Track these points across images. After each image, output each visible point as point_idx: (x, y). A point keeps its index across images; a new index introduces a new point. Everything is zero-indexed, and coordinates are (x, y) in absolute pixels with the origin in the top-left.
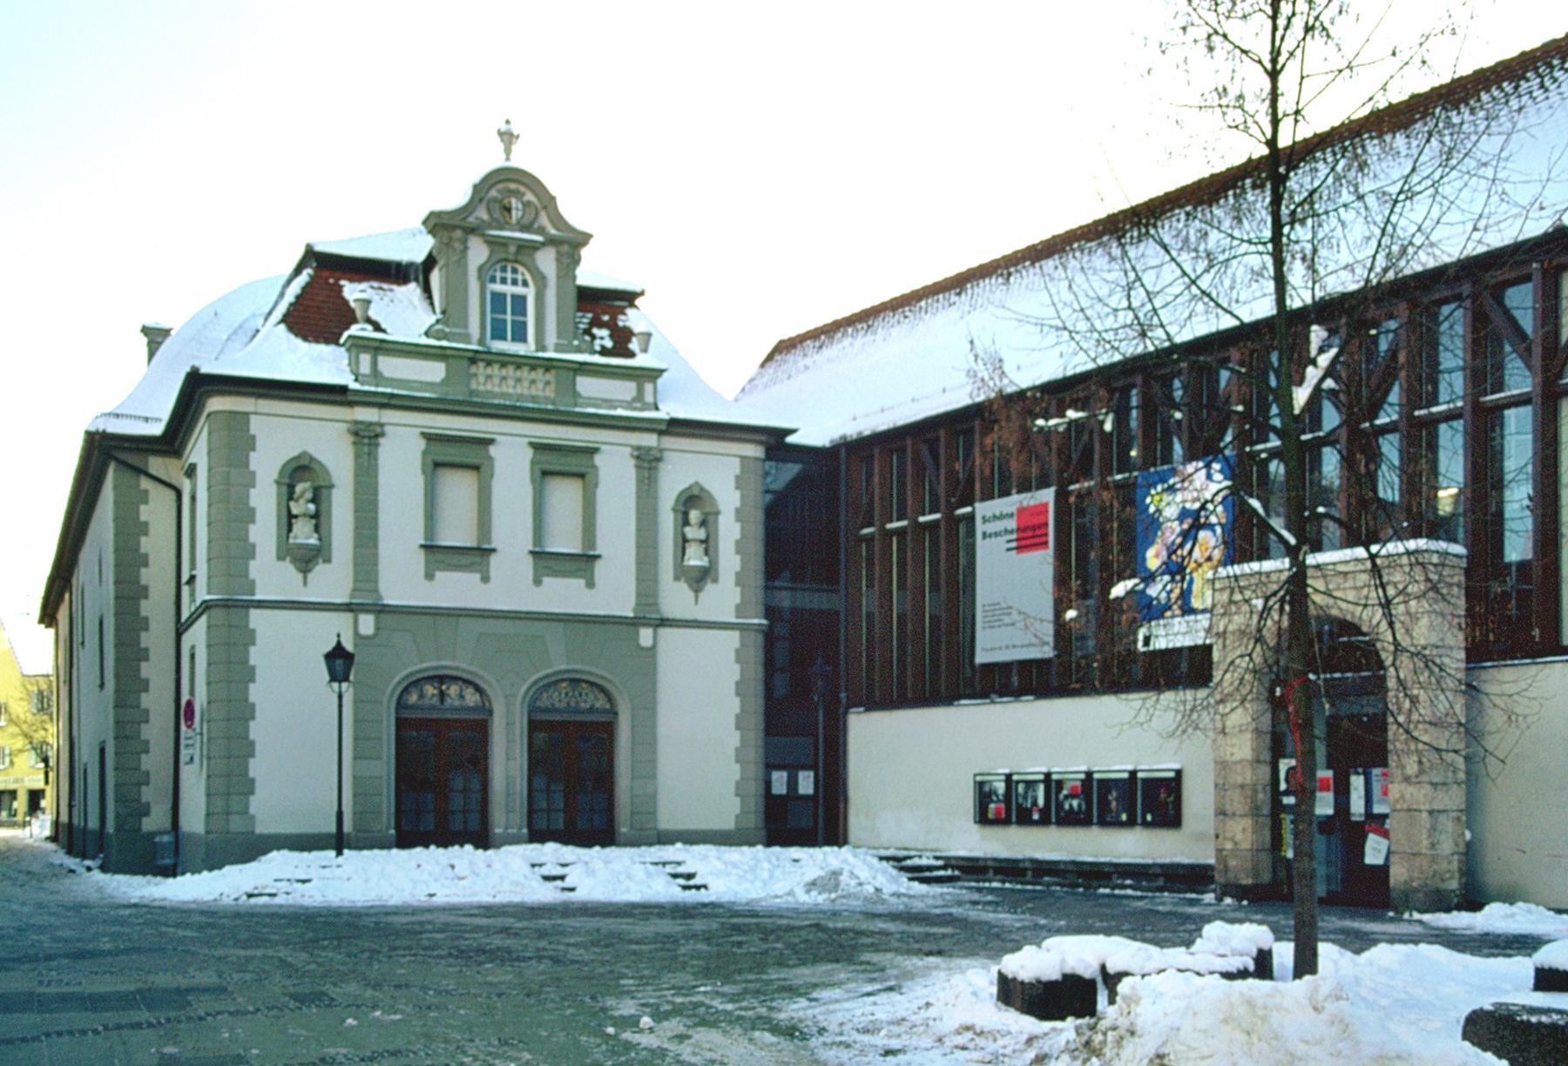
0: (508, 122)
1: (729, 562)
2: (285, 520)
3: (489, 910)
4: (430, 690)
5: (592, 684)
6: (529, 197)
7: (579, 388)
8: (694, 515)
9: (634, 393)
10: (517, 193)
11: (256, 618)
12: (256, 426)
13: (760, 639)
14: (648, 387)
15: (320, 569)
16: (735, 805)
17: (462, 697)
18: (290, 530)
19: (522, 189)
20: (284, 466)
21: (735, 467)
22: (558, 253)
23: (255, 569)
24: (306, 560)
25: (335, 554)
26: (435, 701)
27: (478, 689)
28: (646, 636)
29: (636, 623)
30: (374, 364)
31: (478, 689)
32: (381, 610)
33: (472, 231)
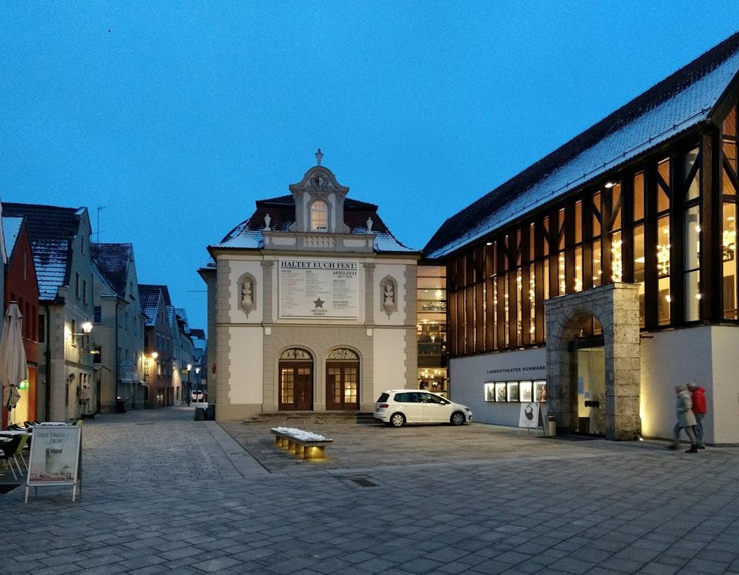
0: (319, 154)
2: (383, 298)
3: (712, 402)
4: (291, 352)
5: (350, 350)
6: (326, 176)
7: (344, 243)
8: (389, 288)
9: (365, 244)
10: (321, 176)
13: (374, 330)
14: (370, 242)
15: (394, 314)
17: (303, 355)
18: (385, 301)
19: (323, 173)
20: (395, 280)
21: (404, 268)
22: (336, 196)
23: (231, 313)
24: (246, 309)
25: (258, 307)
26: (293, 357)
27: (309, 353)
28: (369, 332)
29: (365, 326)
30: (270, 240)
31: (309, 353)
32: (272, 325)
33: (305, 190)
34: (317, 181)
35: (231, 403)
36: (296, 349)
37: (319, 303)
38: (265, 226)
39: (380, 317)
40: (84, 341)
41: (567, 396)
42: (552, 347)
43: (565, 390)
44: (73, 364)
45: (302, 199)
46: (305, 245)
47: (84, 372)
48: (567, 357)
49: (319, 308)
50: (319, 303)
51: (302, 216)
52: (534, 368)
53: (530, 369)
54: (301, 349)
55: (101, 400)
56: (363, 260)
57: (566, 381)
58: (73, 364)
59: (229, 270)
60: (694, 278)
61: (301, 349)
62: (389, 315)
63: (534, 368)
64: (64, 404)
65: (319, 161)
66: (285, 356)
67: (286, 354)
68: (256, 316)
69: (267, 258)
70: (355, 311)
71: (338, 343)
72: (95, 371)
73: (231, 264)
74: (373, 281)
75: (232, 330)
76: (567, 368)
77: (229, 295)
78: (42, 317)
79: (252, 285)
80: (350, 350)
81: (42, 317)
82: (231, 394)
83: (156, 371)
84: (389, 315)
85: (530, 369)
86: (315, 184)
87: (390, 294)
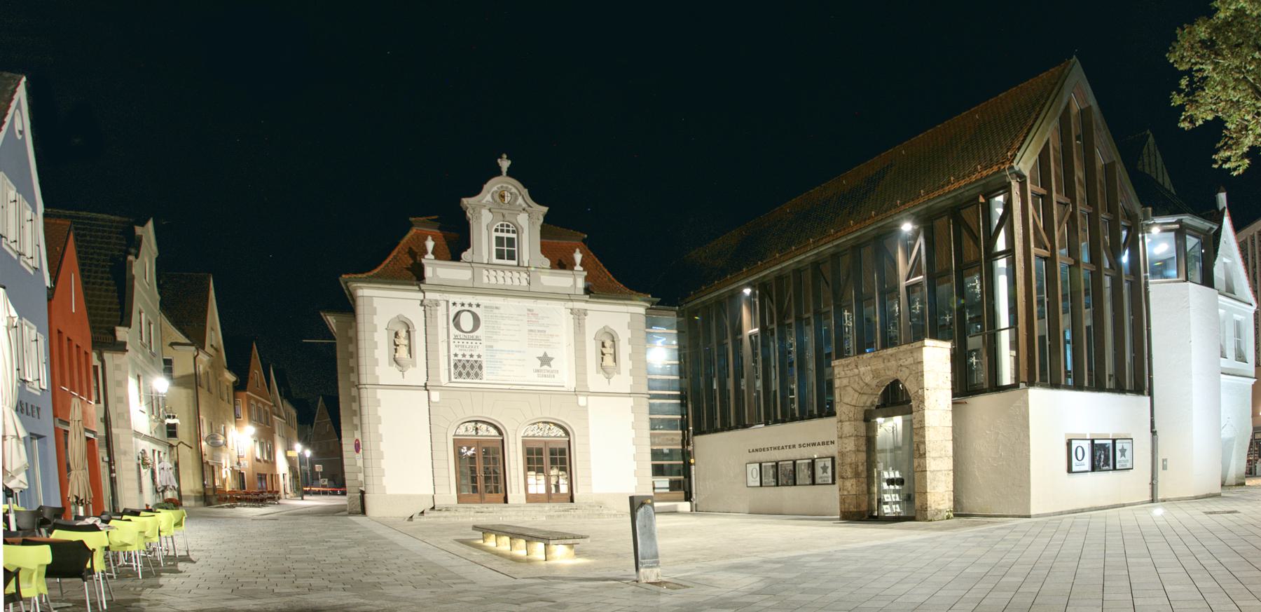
5: (555, 424)
15: (615, 378)
21: (628, 318)
23: (378, 371)
27: (496, 427)
28: (582, 400)
29: (576, 393)
30: (434, 271)
31: (496, 427)
34: (502, 197)
36: (476, 422)
37: (545, 360)
38: (426, 253)
39: (596, 381)
40: (154, 403)
41: (864, 475)
42: (843, 417)
43: (861, 468)
44: (146, 437)
45: (479, 217)
46: (485, 280)
47: (157, 448)
48: (862, 426)
49: (546, 367)
50: (545, 360)
51: (480, 240)
52: (814, 444)
53: (823, 443)
54: (484, 422)
55: (182, 489)
56: (570, 304)
57: (863, 456)
58: (146, 437)
59: (374, 312)
60: (1107, 293)
61: (484, 422)
62: (609, 378)
63: (814, 444)
64: (137, 491)
66: (462, 431)
67: (463, 428)
68: (416, 375)
69: (429, 295)
70: (564, 375)
71: (548, 415)
72: (171, 446)
73: (376, 302)
74: (584, 334)
75: (380, 393)
76: (863, 441)
77: (375, 345)
78: (96, 368)
79: (408, 332)
80: (555, 424)
81: (96, 368)
82: (385, 481)
83: (253, 454)
84: (609, 378)
85: (823, 443)
86: (498, 199)
87: (608, 350)
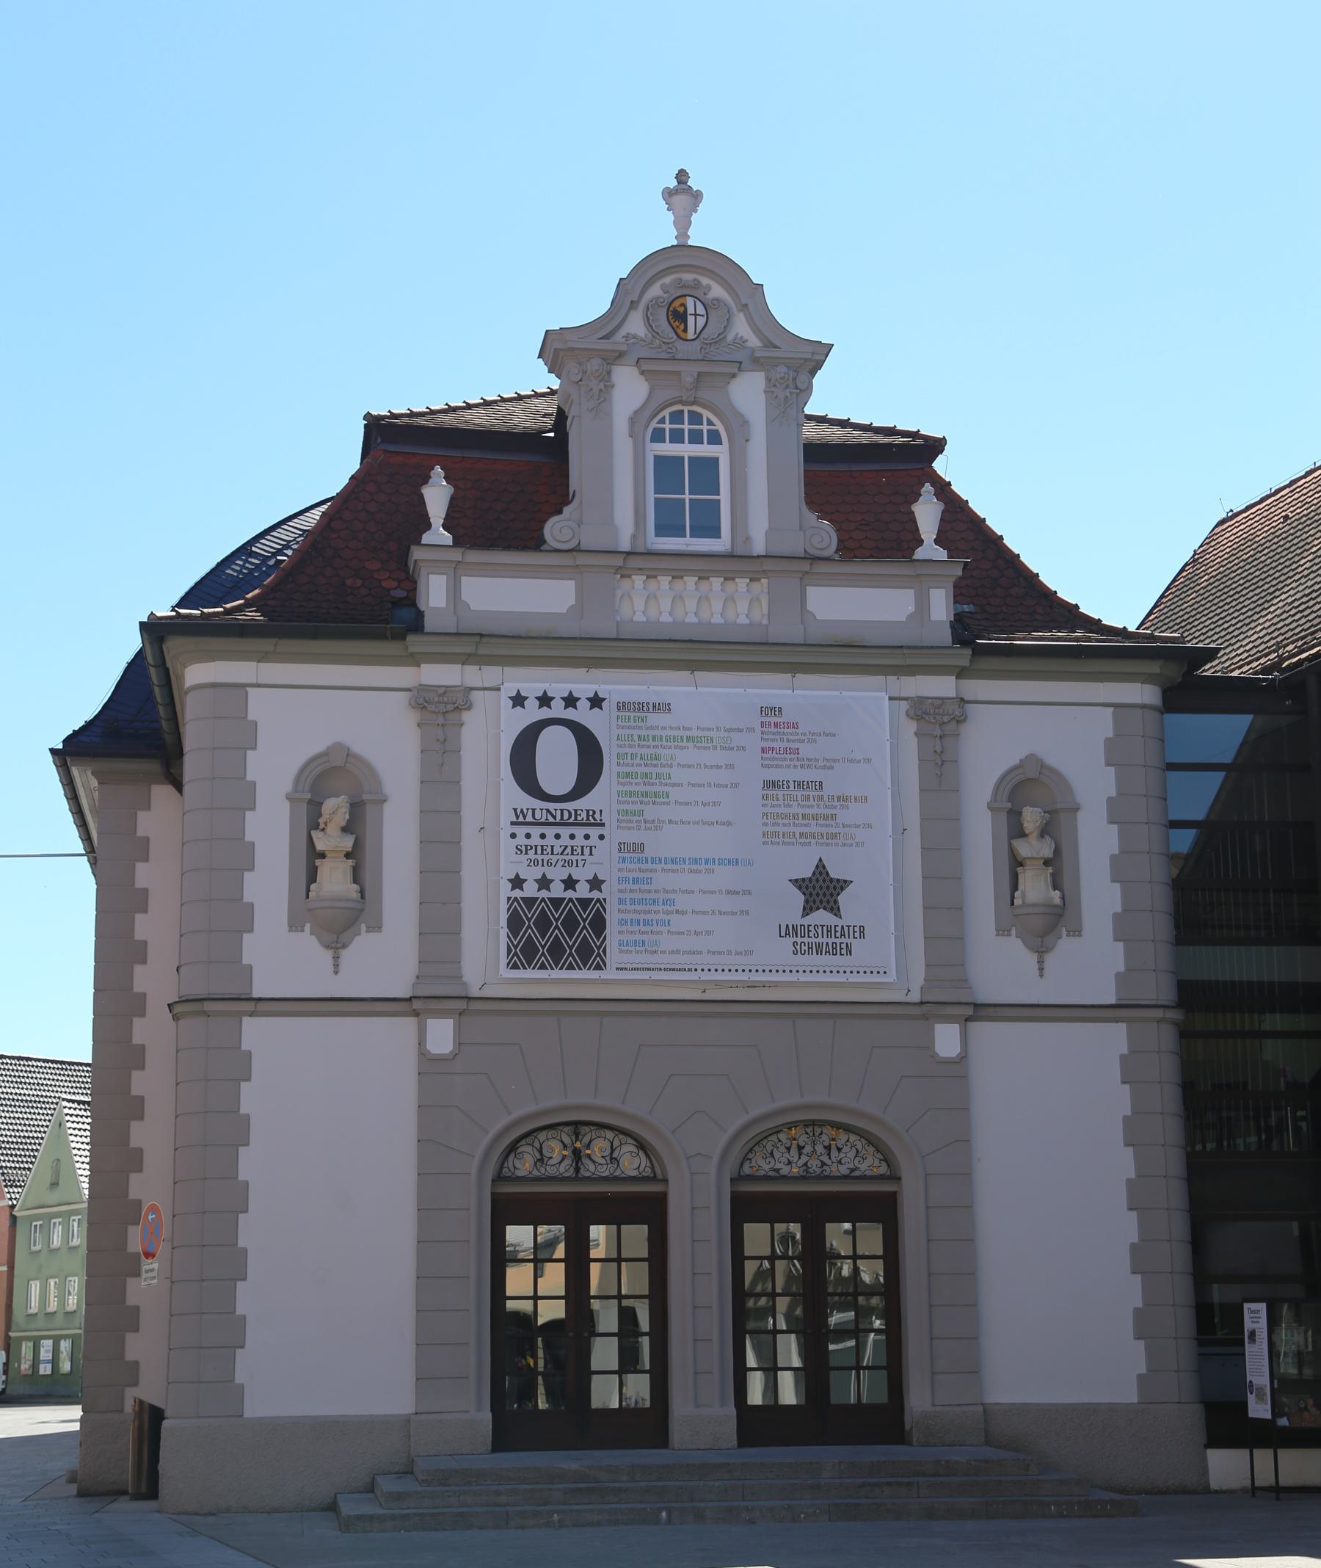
1: (1100, 896)
8: (1032, 819)
11: (255, 1032)
12: (259, 706)
16: (1135, 1358)
35: (248, 1413)
39: (1001, 967)
65: (683, 225)
68: (386, 959)
